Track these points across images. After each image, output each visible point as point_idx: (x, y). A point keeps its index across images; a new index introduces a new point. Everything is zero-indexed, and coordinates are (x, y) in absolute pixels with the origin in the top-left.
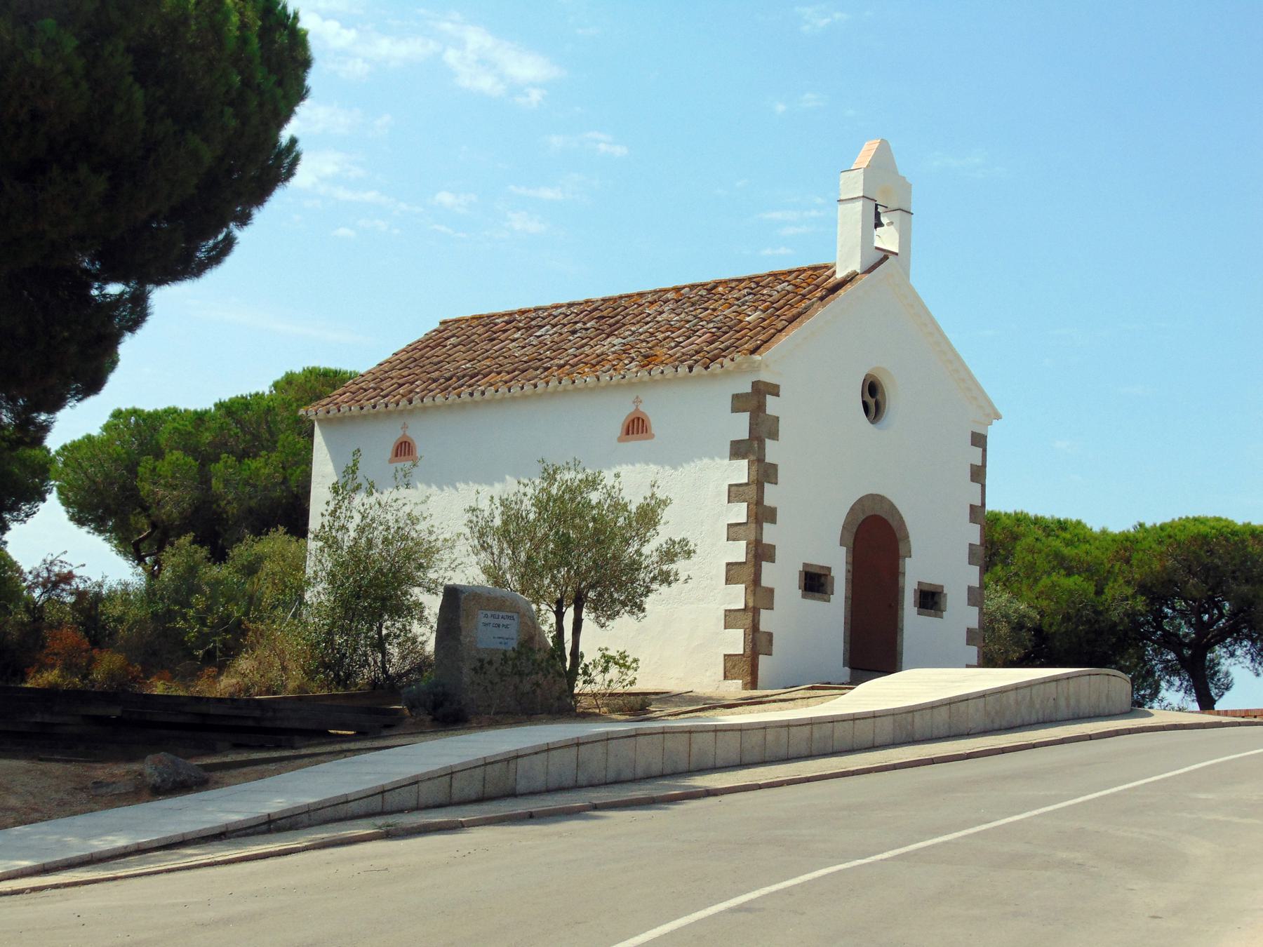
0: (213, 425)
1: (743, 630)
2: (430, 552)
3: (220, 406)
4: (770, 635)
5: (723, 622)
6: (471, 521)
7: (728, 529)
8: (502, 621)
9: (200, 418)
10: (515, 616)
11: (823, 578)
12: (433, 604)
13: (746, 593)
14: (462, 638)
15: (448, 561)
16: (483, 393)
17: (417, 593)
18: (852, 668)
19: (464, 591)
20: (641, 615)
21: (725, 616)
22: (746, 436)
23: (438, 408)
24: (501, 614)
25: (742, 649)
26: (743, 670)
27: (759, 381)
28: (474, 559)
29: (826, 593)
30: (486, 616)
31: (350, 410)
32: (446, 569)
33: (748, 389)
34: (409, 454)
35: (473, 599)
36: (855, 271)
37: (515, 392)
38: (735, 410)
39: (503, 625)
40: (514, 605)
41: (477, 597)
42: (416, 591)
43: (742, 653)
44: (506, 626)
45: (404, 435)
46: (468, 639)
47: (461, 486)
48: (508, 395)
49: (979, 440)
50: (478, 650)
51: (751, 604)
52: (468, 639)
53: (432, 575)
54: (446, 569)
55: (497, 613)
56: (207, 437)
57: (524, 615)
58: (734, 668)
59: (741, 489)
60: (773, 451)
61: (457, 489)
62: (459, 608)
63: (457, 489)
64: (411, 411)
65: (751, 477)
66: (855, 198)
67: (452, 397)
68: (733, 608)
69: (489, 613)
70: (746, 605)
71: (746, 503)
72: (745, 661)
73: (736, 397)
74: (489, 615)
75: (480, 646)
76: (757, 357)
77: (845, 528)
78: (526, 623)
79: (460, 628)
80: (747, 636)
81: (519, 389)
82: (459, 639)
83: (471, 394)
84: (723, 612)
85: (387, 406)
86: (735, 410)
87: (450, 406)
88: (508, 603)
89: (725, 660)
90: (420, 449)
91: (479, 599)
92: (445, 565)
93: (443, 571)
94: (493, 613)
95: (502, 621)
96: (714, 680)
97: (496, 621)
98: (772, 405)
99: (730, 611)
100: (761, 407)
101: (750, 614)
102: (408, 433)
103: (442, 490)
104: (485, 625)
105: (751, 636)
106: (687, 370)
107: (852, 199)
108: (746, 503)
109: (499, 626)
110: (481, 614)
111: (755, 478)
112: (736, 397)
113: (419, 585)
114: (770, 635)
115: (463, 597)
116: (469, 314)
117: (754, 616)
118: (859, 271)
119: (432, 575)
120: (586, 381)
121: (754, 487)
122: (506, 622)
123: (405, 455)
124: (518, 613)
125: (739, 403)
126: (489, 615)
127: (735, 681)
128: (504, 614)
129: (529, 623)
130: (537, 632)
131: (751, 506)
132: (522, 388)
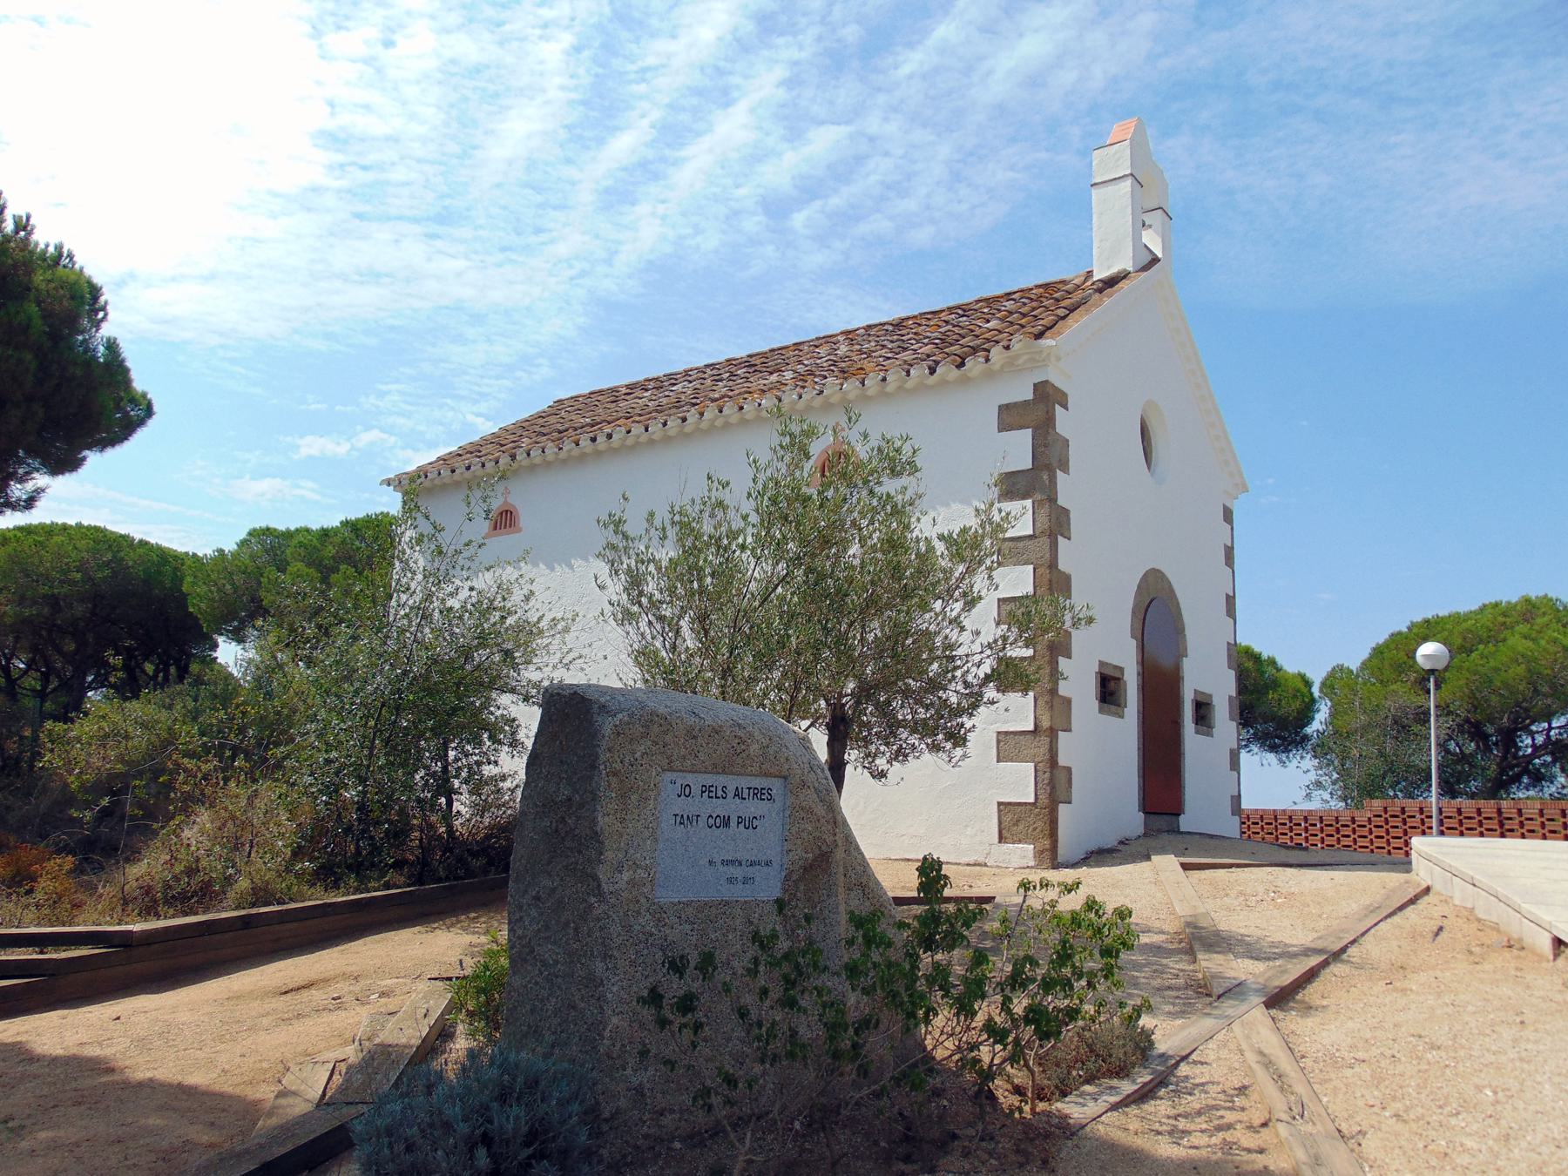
0: (338, 540)
1: (1031, 765)
2: (528, 632)
3: (346, 523)
4: (1069, 770)
5: (994, 751)
6: (613, 547)
7: (999, 607)
8: (732, 807)
9: (325, 533)
10: (776, 785)
11: (1112, 683)
12: (529, 719)
13: (1035, 706)
14: (603, 873)
15: (558, 655)
16: (610, 436)
17: (507, 704)
18: (1146, 813)
19: (613, 706)
20: (959, 752)
21: (998, 742)
22: (1027, 463)
23: (548, 465)
24: (732, 782)
25: (1033, 795)
26: (1035, 829)
27: (1046, 382)
28: (614, 632)
29: (1119, 706)
30: (685, 791)
31: (440, 473)
32: (555, 667)
33: (1029, 396)
34: (510, 526)
35: (646, 735)
36: (1125, 270)
37: (654, 433)
38: (1004, 427)
39: (740, 820)
40: (771, 750)
41: (655, 729)
42: (505, 699)
43: (1032, 800)
44: (748, 823)
45: (506, 502)
46: (626, 876)
47: (576, 563)
48: (644, 437)
49: (1228, 516)
50: (659, 913)
51: (1046, 723)
52: (626, 876)
53: (530, 674)
54: (555, 667)
55: (720, 780)
56: (330, 551)
57: (804, 784)
58: (1016, 823)
59: (1021, 544)
60: (1068, 490)
61: (571, 567)
62: (593, 767)
63: (571, 567)
64: (515, 472)
65: (1038, 525)
66: (1119, 178)
67: (568, 445)
68: (1011, 730)
69: (696, 781)
70: (1035, 724)
71: (1032, 566)
72: (1038, 815)
73: (1005, 409)
74: (696, 789)
75: (666, 896)
76: (1047, 342)
77: (1134, 613)
78: (810, 811)
79: (596, 836)
80: (1040, 773)
81: (660, 425)
82: (595, 878)
83: (594, 440)
84: (995, 735)
85: (483, 465)
86: (1004, 427)
87: (564, 461)
88: (754, 748)
89: (999, 811)
90: (524, 518)
91: (666, 732)
92: (555, 659)
93: (550, 668)
94: (709, 779)
95: (732, 807)
96: (981, 843)
97: (719, 808)
98: (1064, 422)
99: (1007, 733)
100: (1050, 420)
101: (1045, 740)
102: (509, 500)
103: (552, 569)
104: (684, 820)
105: (1047, 775)
106: (927, 371)
107: (1115, 179)
108: (1032, 566)
109: (726, 822)
110: (670, 783)
111: (1046, 527)
112: (1005, 409)
113: (513, 691)
114: (1069, 770)
115: (607, 726)
116: (586, 391)
117: (1051, 742)
118: (1131, 269)
119: (530, 674)
120: (760, 405)
121: (1045, 541)
122: (753, 807)
123: (505, 527)
124: (785, 778)
125: (1009, 416)
126: (696, 789)
127: (1021, 846)
128: (744, 782)
129: (820, 810)
130: (839, 839)
131: (1040, 571)
132: (665, 424)
